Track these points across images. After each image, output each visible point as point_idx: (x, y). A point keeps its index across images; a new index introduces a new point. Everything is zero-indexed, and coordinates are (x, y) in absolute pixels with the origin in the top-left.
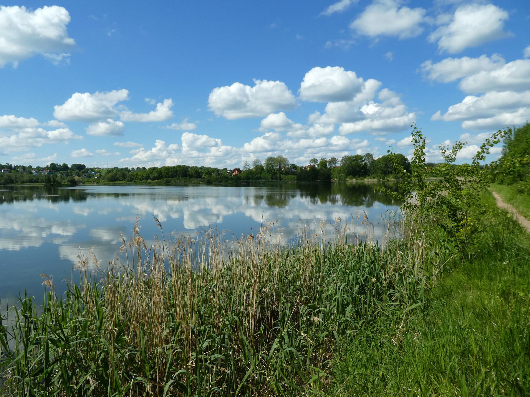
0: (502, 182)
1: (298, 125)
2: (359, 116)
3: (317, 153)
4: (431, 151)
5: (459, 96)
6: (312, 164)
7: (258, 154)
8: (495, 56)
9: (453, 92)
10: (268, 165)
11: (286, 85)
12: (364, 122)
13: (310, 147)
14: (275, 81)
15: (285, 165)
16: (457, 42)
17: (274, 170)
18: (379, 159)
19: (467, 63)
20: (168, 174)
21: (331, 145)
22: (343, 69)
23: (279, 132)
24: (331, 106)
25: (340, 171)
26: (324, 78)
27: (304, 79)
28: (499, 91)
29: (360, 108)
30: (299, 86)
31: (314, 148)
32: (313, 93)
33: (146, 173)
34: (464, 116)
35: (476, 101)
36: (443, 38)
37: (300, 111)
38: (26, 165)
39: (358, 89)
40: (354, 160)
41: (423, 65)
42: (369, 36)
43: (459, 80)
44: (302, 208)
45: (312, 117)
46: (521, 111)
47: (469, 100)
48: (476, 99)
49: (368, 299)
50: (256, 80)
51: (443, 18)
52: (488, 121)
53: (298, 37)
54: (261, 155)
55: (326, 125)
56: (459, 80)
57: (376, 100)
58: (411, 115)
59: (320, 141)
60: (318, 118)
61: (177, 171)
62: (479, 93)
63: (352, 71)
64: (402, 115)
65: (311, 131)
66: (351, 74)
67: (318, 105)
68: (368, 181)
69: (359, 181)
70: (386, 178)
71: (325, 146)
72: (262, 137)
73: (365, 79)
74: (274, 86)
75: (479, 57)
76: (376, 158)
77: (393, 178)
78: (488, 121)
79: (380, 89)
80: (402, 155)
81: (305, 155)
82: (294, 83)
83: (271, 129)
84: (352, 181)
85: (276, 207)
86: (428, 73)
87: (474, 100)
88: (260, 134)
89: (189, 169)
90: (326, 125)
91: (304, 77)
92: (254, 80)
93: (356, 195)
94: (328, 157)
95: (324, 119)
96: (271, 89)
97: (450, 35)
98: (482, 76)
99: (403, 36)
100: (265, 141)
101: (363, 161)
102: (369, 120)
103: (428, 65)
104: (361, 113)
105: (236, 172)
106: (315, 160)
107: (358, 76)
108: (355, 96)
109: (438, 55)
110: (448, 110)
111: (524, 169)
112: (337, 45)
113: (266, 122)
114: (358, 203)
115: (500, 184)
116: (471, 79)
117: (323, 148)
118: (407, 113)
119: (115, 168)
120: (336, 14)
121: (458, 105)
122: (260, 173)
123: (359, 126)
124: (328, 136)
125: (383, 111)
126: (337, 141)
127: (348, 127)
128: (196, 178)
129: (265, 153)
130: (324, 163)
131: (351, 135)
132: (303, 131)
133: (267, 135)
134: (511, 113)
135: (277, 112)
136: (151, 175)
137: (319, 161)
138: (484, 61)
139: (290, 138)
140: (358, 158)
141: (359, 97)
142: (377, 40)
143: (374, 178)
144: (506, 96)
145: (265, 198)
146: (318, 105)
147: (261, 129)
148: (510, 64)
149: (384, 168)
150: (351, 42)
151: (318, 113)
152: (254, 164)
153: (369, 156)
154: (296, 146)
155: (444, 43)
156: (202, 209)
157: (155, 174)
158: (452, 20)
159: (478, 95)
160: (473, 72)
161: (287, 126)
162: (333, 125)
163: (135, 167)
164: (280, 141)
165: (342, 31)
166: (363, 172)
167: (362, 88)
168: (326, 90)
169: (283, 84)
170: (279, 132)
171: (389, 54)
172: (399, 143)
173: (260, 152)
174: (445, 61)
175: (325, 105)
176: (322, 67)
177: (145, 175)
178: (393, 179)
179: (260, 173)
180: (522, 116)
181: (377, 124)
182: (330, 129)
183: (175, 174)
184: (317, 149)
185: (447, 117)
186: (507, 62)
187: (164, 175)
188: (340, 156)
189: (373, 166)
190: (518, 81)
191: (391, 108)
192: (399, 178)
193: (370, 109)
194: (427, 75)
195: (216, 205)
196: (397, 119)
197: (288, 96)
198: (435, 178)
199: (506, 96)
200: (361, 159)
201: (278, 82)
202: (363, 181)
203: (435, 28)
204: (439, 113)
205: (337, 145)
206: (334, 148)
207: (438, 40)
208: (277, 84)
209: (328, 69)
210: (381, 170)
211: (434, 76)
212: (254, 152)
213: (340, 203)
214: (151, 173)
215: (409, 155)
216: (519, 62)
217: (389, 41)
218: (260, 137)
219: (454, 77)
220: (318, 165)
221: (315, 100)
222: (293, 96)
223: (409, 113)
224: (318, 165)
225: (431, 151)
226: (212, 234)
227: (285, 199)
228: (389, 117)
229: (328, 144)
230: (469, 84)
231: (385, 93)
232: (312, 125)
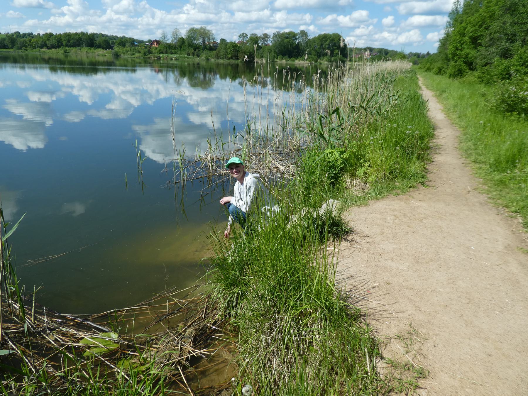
0: (440, 72)
15: (209, 39)
18: (315, 38)
20: (69, 41)
25: (270, 51)
33: (41, 40)
40: (287, 38)
44: (227, 90)
61: (80, 39)
68: (298, 63)
69: (290, 62)
70: (319, 60)
76: (311, 37)
77: (326, 61)
84: (282, 62)
89: (95, 36)
93: (285, 79)
94: (259, 33)
101: (296, 39)
105: (155, 45)
106: (243, 35)
111: (475, 51)
114: (287, 87)
115: (437, 74)
119: (16, 33)
128: (103, 48)
130: (255, 40)
136: (47, 42)
137: (249, 36)
140: (291, 36)
149: (319, 48)
152: (173, 35)
153: (304, 33)
156: (123, 91)
157: (53, 41)
163: (42, 33)
166: (296, 52)
177: (40, 43)
178: (326, 63)
183: (77, 43)
187: (64, 43)
188: (271, 32)
189: (307, 46)
195: (152, 85)
200: (294, 36)
202: (293, 63)
210: (316, 51)
213: (270, 87)
214: (49, 40)
226: (146, 114)
227: (210, 80)
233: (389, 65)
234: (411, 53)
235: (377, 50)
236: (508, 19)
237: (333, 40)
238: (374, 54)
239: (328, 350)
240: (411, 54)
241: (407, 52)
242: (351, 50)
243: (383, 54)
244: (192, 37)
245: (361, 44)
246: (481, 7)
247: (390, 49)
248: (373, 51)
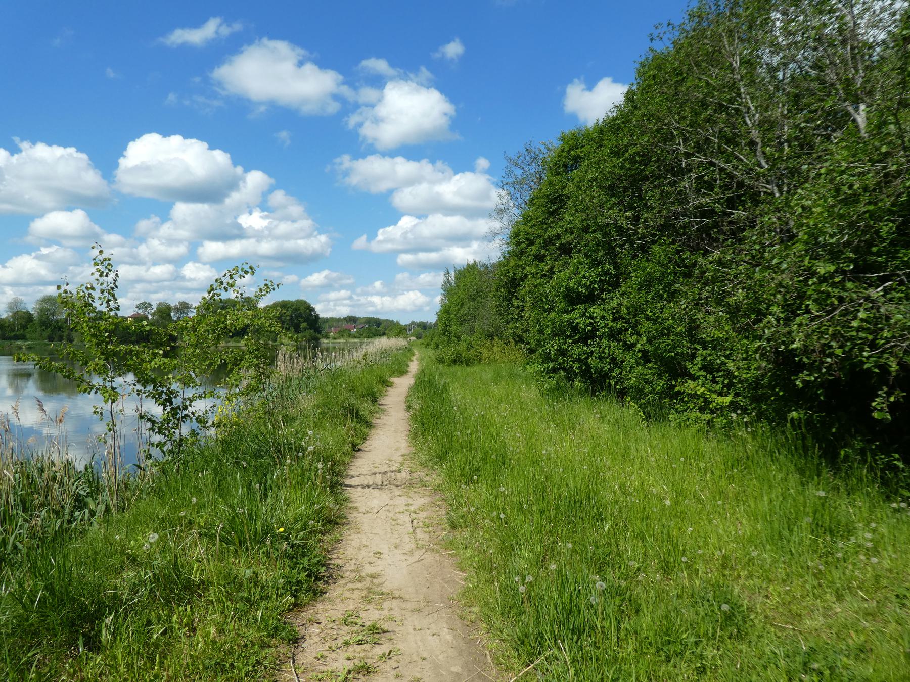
2: (235, 232)
3: (156, 292)
4: (355, 297)
5: (394, 217)
6: (140, 312)
7: (23, 289)
8: (439, 164)
9: (382, 208)
10: (43, 311)
11: (90, 159)
12: (244, 242)
13: (139, 281)
14: (65, 146)
16: (389, 133)
17: (57, 321)
19: (403, 167)
21: (183, 278)
22: (205, 145)
23: (73, 248)
24: (182, 209)
26: (160, 156)
27: (125, 153)
28: (446, 215)
29: (236, 218)
30: (116, 165)
31: (149, 282)
32: (144, 180)
34: (400, 247)
35: (415, 226)
36: (367, 124)
37: (121, 211)
39: (233, 185)
41: (337, 160)
42: (249, 100)
43: (391, 192)
45: (143, 225)
46: (475, 245)
47: (406, 222)
48: (417, 221)
50: (22, 140)
51: (368, 94)
52: (433, 256)
53: (110, 73)
54: (31, 290)
55: (171, 241)
56: (391, 192)
57: (264, 205)
58: (323, 238)
59: (159, 271)
60: (157, 227)
62: (421, 214)
63: (225, 151)
64: (309, 236)
65: (143, 250)
66: (221, 157)
67: (159, 203)
71: (169, 281)
72: (33, 254)
73: (247, 170)
74: (62, 156)
78: (433, 256)
79: (271, 190)
80: (305, 302)
81: (130, 295)
82: (106, 158)
83: (54, 239)
85: (62, 395)
86: (347, 173)
87: (413, 224)
88: (29, 249)
90: (171, 241)
91: (125, 149)
92: (16, 139)
94: (174, 299)
95: (166, 229)
96: (53, 161)
97: (377, 121)
98: (422, 189)
99: (306, 109)
100: (41, 263)
102: (253, 241)
103: (346, 160)
104: (239, 227)
106: (146, 305)
107: (235, 163)
108: (226, 195)
109: (363, 149)
110: (376, 236)
112: (187, 103)
113: (41, 226)
116: (407, 191)
117: (166, 283)
118: (316, 233)
120: (186, 49)
121: (391, 228)
122: (24, 327)
123: (235, 248)
124: (178, 262)
125: (276, 226)
127: (213, 249)
129: (41, 288)
130: (164, 312)
132: (126, 250)
133: (45, 251)
134: (463, 247)
135: (70, 209)
137: (155, 307)
138: (425, 168)
141: (234, 198)
142: (263, 108)
144: (454, 223)
145: (36, 376)
147: (29, 239)
148: (457, 177)
150: (216, 103)
151: (157, 219)
152: (10, 308)
155: (368, 131)
158: (380, 100)
159: (419, 217)
160: (411, 182)
162: (186, 243)
164: (77, 265)
165: (197, 79)
167: (241, 184)
168: (170, 179)
169: (84, 156)
170: (73, 248)
171: (284, 135)
172: (304, 282)
173: (27, 285)
174: (370, 158)
175: (170, 206)
176: (185, 137)
179: (24, 327)
180: (475, 253)
181: (266, 247)
182: (182, 249)
184: (154, 285)
185: (375, 246)
186: (456, 173)
190: (469, 203)
191: (289, 223)
193: (254, 221)
194: (344, 177)
196: (301, 242)
197: (91, 179)
198: (356, 340)
199: (454, 223)
201: (71, 150)
202: (238, 344)
203: (356, 106)
204: (364, 238)
205: (194, 280)
207: (361, 125)
208: (70, 155)
209: (176, 140)
211: (354, 180)
212: (14, 284)
215: (319, 302)
216: (469, 175)
217: (283, 115)
218: (30, 254)
219: (384, 186)
220: (153, 314)
221: (148, 195)
222: (105, 182)
223: (320, 234)
224: (153, 314)
225: (355, 297)
228: (287, 237)
229: (177, 277)
230: (405, 198)
231: (279, 197)
232: (142, 240)
233: (382, 342)
234: (413, 323)
235: (363, 321)
236: (472, 305)
237: (296, 310)
238: (360, 326)
239: (881, 16)
240: (414, 325)
241: (405, 321)
242: (326, 320)
243: (375, 327)
244: (48, 310)
245: (343, 311)
246: (705, 155)
247: (382, 317)
248: (358, 322)
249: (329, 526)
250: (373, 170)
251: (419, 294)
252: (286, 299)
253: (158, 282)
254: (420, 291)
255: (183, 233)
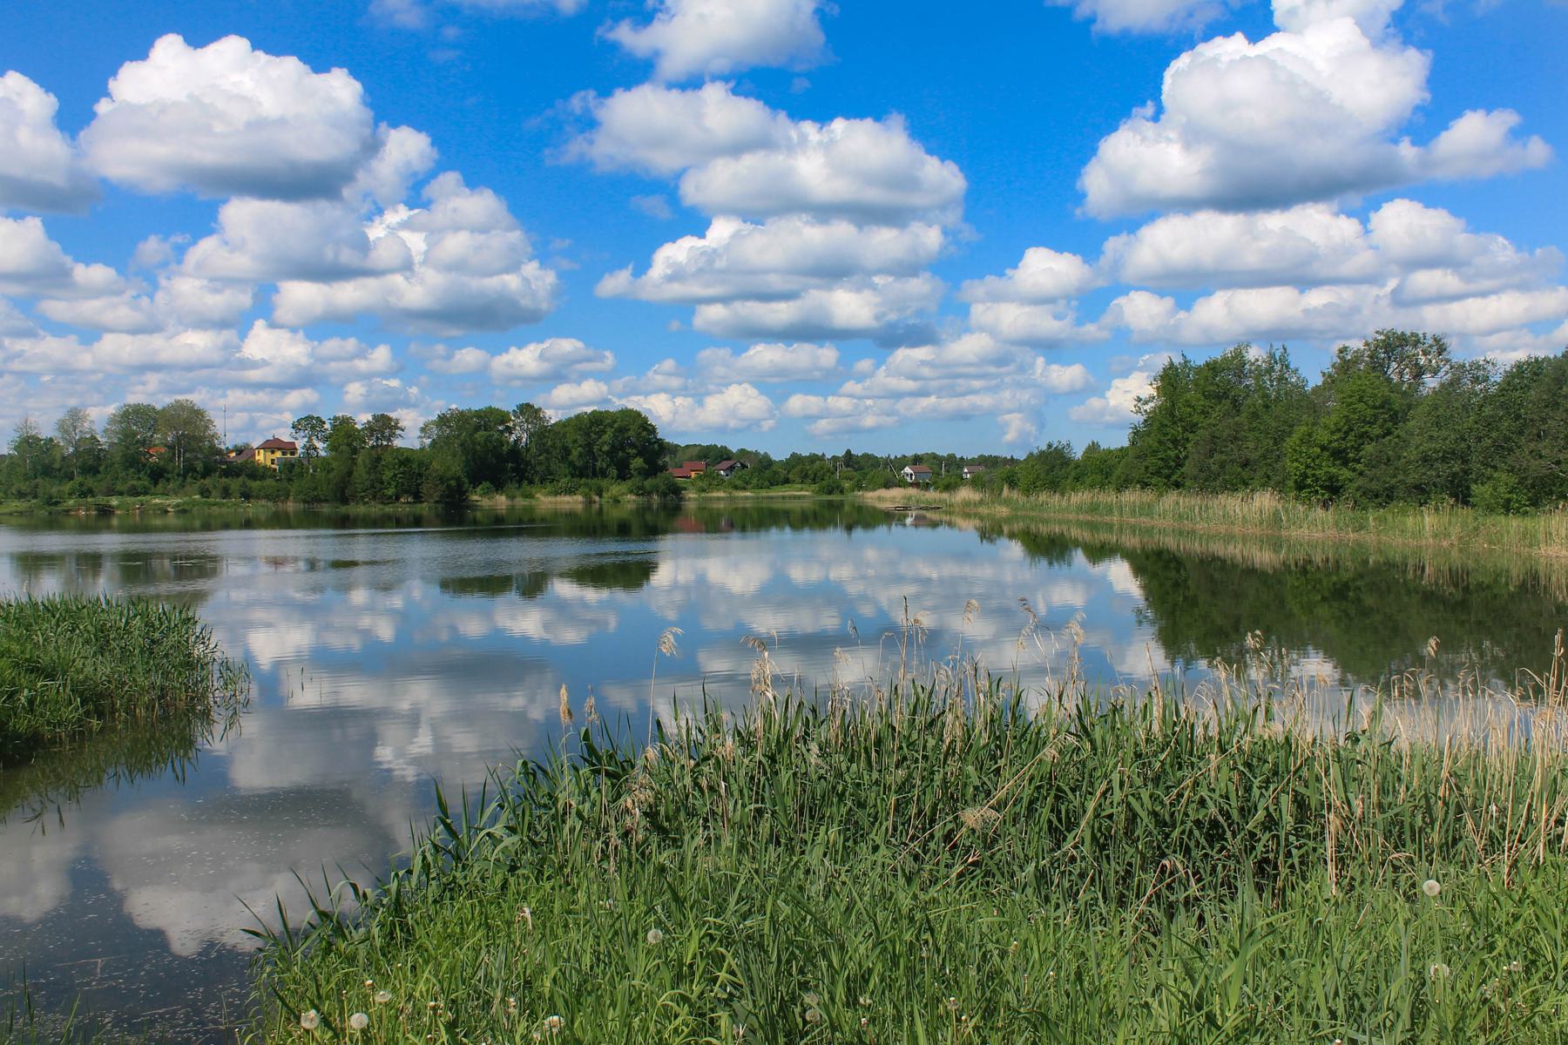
1: (98, 274)
2: (347, 257)
8: (948, 162)
38: (943, 453)
47: (721, 231)
49: (1289, 995)
55: (221, 282)
59: (197, 342)
75: (1427, 207)
91: (114, 74)
101: (509, 430)
123: (348, 294)
124: (239, 323)
126: (267, 346)
127: (301, 295)
131: (319, 327)
139: (60, 329)
140: (491, 419)
143: (570, 491)
144: (811, 237)
146: (190, 205)
154: (85, 359)
161: (52, 278)
166: (513, 470)
190: (874, 195)
192: (649, 493)
205: (264, 363)
206: (254, 375)
209: (233, 47)
230: (716, 181)
237: (622, 430)
249: (936, 730)
250: (635, 114)
251: (752, 391)
252: (463, 406)
253: (189, 367)
254: (754, 384)
255: (242, 263)
